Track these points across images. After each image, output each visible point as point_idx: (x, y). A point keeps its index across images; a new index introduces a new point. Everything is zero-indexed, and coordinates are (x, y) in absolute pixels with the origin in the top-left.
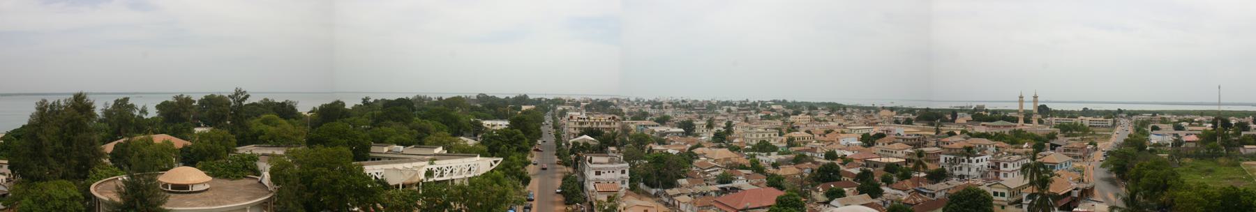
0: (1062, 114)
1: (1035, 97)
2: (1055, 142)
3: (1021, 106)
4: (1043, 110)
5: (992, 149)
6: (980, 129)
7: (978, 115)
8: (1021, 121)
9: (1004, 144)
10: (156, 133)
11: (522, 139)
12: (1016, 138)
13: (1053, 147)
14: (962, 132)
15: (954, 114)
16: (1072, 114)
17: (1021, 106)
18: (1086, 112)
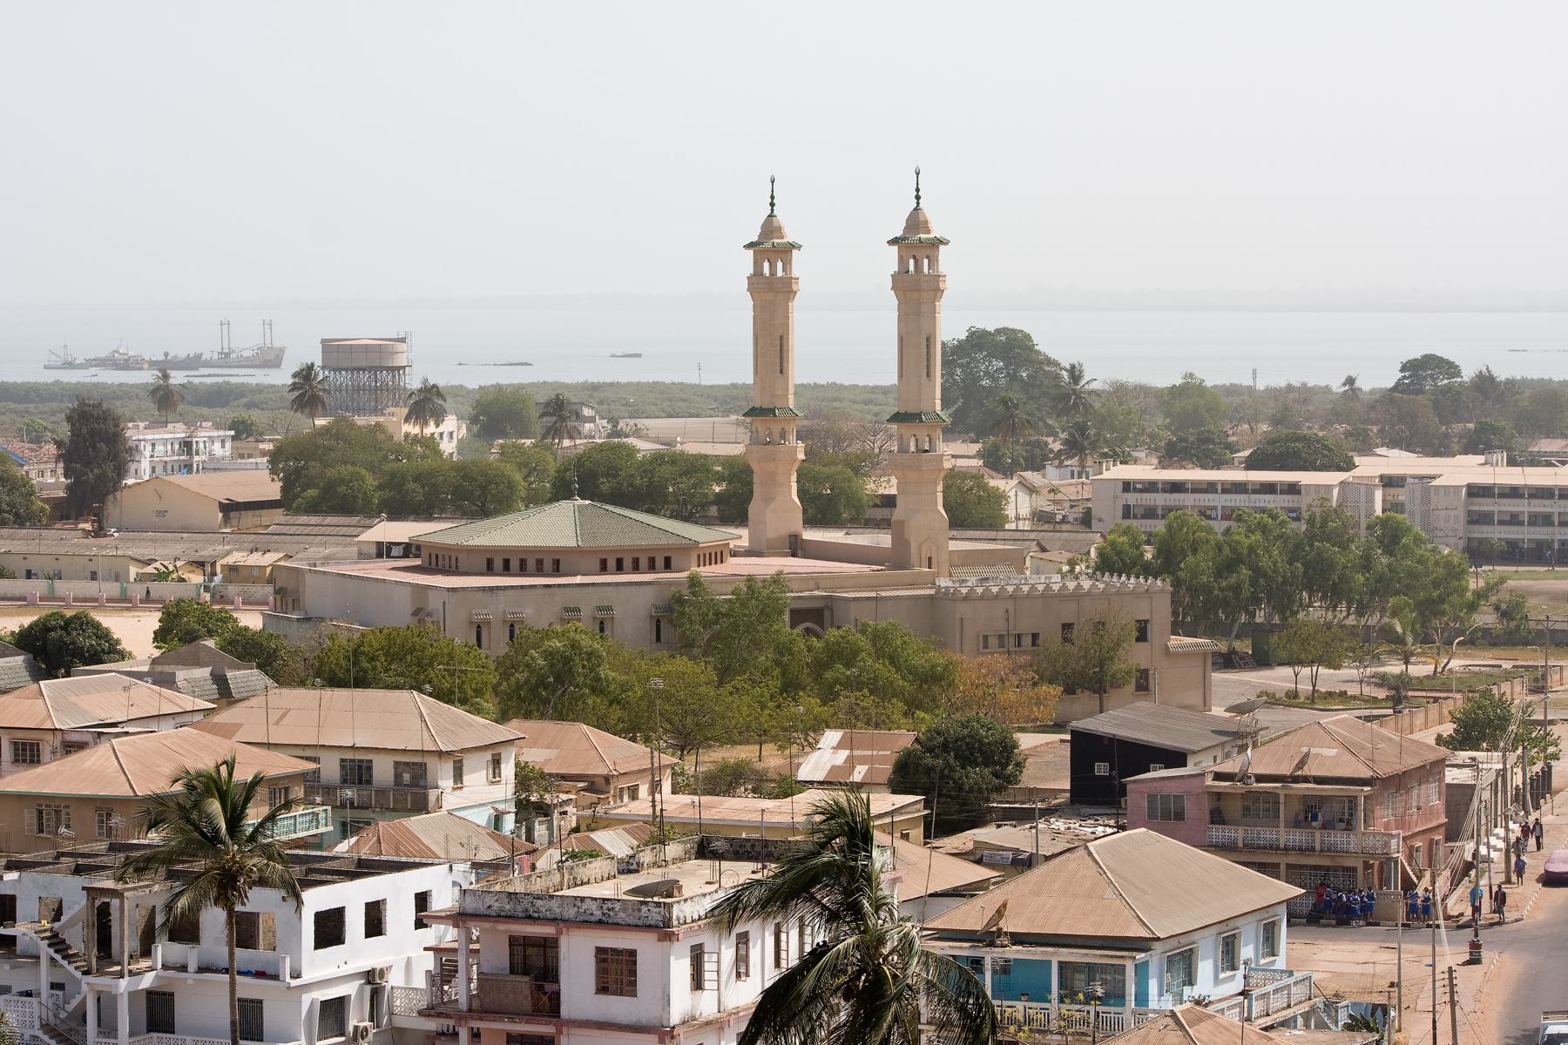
0: (1192, 422)
1: (916, 244)
2: (1121, 719)
3: (772, 343)
4: (1007, 396)
5: (475, 798)
6: (360, 563)
7: (338, 445)
8: (782, 506)
9: (613, 752)
10: (1023, 730)
12: (729, 669)
13: (1106, 777)
14: (178, 632)
15: (93, 442)
16: (1300, 432)
17: (772, 343)
18: (1433, 403)
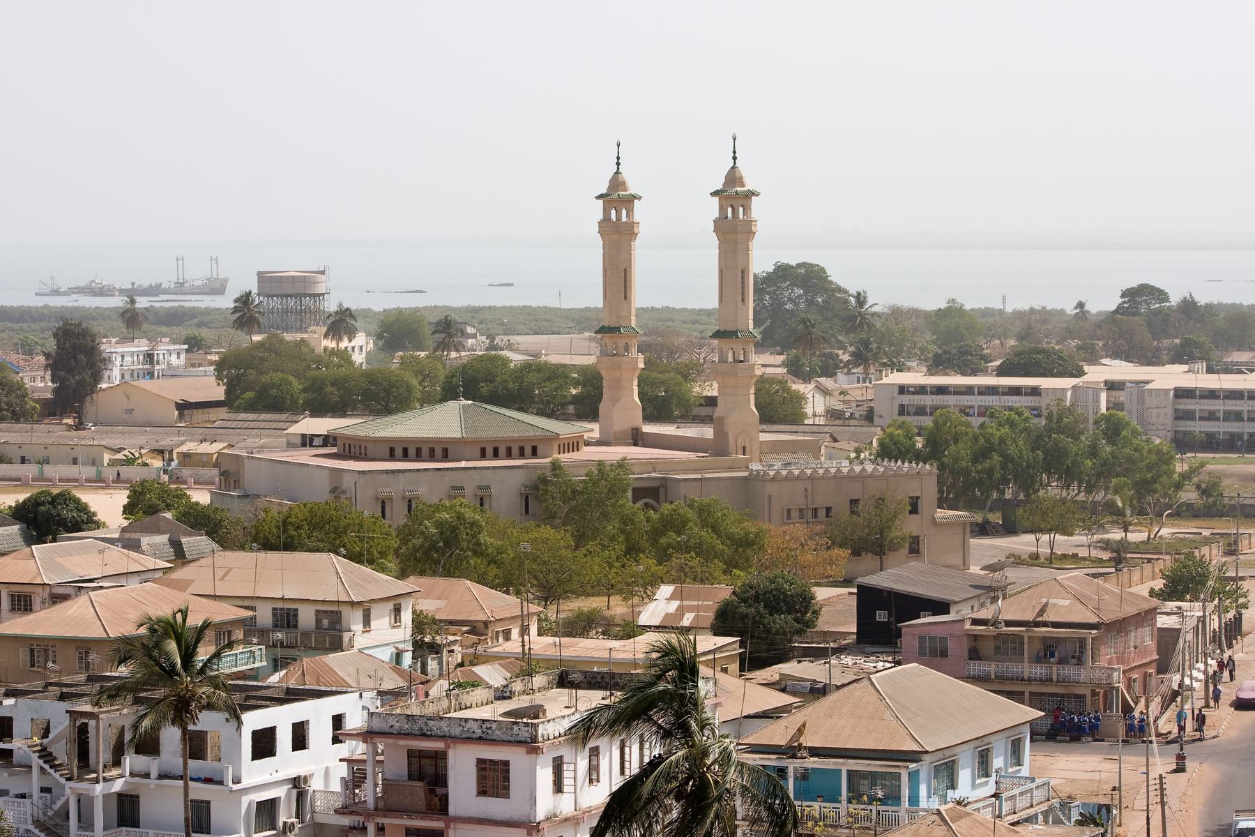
0: (954, 338)
1: (734, 195)
2: (897, 576)
3: (618, 275)
4: (806, 317)
5: (380, 639)
6: (288, 451)
7: (271, 357)
8: (626, 405)
9: (490, 602)
11: (1088, 492)
12: (583, 536)
13: (885, 623)
14: (142, 506)
15: (75, 354)
16: (1040, 346)
17: (618, 275)
18: (1147, 323)
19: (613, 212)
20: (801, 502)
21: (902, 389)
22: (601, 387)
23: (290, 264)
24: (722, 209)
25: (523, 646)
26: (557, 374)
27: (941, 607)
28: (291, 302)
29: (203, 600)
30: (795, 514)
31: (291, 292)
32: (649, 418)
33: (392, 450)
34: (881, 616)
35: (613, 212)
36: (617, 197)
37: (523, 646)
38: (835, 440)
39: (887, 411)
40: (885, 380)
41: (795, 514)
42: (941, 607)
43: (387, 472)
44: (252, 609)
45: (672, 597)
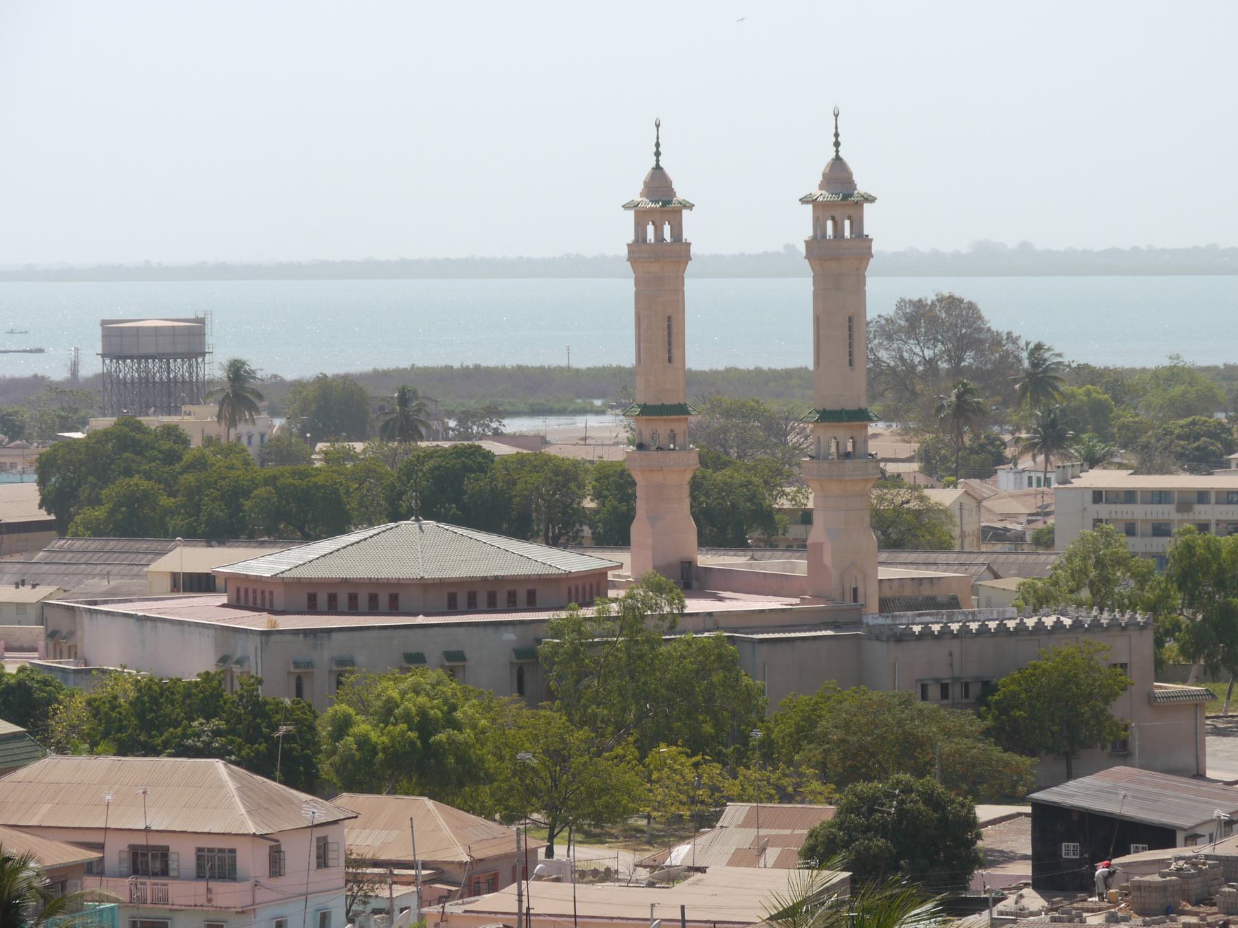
1: (840, 196)
3: (660, 318)
4: (979, 390)
6: (168, 608)
8: (666, 525)
17: (660, 318)
19: (650, 229)
20: (944, 673)
21: (1098, 496)
22: (633, 497)
23: (154, 308)
24: (818, 224)
25: (520, 901)
26: (566, 476)
27: (1162, 836)
28: (154, 366)
29: (14, 833)
30: (934, 691)
31: (151, 350)
32: (708, 541)
33: (312, 598)
34: (1069, 850)
35: (650, 229)
36: (660, 200)
37: (520, 901)
38: (997, 576)
39: (1072, 533)
40: (1076, 483)
41: (956, 692)
42: (1162, 836)
43: (306, 633)
44: (99, 847)
45: (745, 824)
